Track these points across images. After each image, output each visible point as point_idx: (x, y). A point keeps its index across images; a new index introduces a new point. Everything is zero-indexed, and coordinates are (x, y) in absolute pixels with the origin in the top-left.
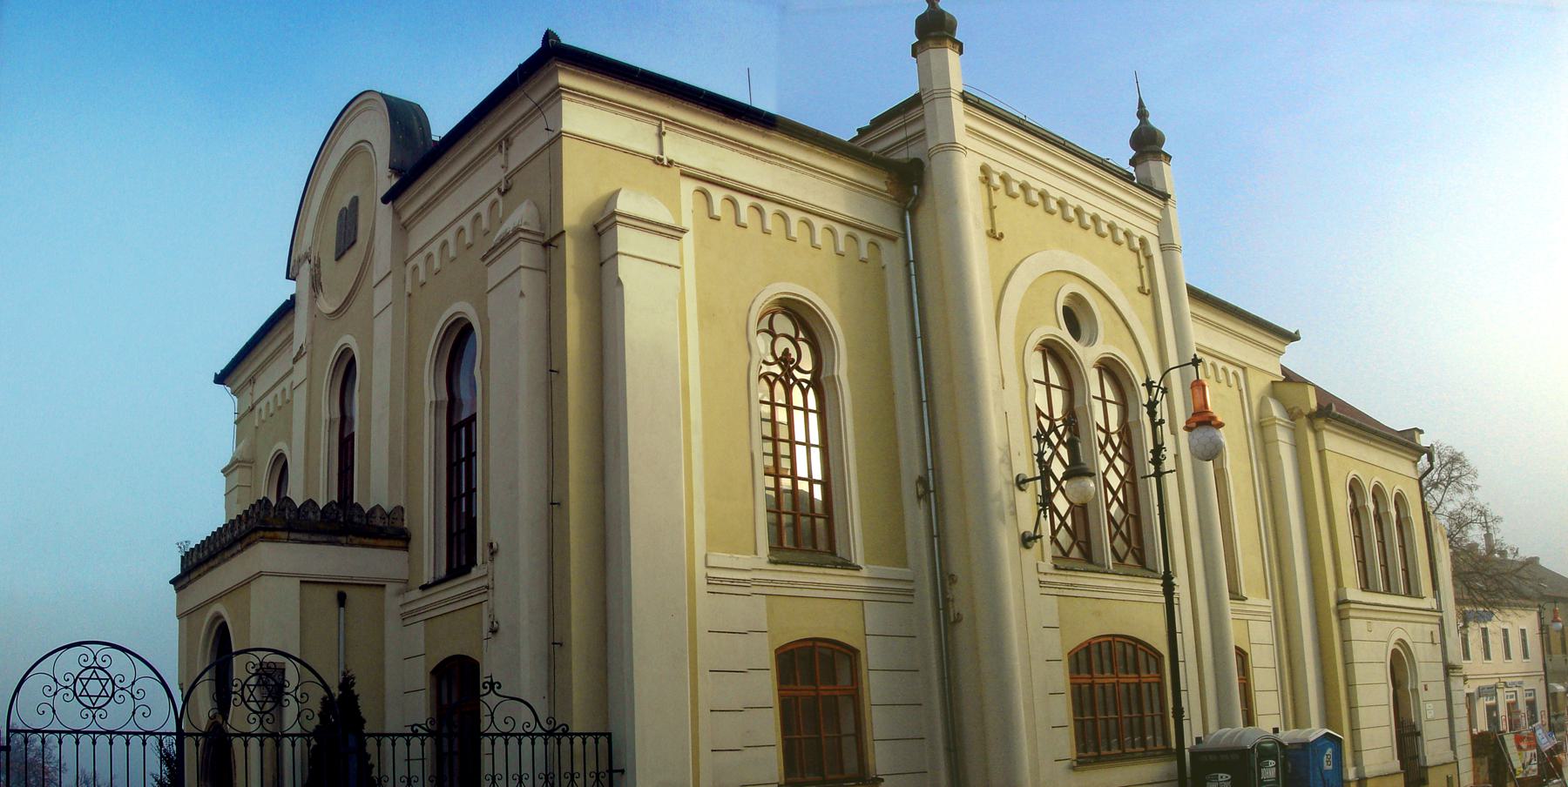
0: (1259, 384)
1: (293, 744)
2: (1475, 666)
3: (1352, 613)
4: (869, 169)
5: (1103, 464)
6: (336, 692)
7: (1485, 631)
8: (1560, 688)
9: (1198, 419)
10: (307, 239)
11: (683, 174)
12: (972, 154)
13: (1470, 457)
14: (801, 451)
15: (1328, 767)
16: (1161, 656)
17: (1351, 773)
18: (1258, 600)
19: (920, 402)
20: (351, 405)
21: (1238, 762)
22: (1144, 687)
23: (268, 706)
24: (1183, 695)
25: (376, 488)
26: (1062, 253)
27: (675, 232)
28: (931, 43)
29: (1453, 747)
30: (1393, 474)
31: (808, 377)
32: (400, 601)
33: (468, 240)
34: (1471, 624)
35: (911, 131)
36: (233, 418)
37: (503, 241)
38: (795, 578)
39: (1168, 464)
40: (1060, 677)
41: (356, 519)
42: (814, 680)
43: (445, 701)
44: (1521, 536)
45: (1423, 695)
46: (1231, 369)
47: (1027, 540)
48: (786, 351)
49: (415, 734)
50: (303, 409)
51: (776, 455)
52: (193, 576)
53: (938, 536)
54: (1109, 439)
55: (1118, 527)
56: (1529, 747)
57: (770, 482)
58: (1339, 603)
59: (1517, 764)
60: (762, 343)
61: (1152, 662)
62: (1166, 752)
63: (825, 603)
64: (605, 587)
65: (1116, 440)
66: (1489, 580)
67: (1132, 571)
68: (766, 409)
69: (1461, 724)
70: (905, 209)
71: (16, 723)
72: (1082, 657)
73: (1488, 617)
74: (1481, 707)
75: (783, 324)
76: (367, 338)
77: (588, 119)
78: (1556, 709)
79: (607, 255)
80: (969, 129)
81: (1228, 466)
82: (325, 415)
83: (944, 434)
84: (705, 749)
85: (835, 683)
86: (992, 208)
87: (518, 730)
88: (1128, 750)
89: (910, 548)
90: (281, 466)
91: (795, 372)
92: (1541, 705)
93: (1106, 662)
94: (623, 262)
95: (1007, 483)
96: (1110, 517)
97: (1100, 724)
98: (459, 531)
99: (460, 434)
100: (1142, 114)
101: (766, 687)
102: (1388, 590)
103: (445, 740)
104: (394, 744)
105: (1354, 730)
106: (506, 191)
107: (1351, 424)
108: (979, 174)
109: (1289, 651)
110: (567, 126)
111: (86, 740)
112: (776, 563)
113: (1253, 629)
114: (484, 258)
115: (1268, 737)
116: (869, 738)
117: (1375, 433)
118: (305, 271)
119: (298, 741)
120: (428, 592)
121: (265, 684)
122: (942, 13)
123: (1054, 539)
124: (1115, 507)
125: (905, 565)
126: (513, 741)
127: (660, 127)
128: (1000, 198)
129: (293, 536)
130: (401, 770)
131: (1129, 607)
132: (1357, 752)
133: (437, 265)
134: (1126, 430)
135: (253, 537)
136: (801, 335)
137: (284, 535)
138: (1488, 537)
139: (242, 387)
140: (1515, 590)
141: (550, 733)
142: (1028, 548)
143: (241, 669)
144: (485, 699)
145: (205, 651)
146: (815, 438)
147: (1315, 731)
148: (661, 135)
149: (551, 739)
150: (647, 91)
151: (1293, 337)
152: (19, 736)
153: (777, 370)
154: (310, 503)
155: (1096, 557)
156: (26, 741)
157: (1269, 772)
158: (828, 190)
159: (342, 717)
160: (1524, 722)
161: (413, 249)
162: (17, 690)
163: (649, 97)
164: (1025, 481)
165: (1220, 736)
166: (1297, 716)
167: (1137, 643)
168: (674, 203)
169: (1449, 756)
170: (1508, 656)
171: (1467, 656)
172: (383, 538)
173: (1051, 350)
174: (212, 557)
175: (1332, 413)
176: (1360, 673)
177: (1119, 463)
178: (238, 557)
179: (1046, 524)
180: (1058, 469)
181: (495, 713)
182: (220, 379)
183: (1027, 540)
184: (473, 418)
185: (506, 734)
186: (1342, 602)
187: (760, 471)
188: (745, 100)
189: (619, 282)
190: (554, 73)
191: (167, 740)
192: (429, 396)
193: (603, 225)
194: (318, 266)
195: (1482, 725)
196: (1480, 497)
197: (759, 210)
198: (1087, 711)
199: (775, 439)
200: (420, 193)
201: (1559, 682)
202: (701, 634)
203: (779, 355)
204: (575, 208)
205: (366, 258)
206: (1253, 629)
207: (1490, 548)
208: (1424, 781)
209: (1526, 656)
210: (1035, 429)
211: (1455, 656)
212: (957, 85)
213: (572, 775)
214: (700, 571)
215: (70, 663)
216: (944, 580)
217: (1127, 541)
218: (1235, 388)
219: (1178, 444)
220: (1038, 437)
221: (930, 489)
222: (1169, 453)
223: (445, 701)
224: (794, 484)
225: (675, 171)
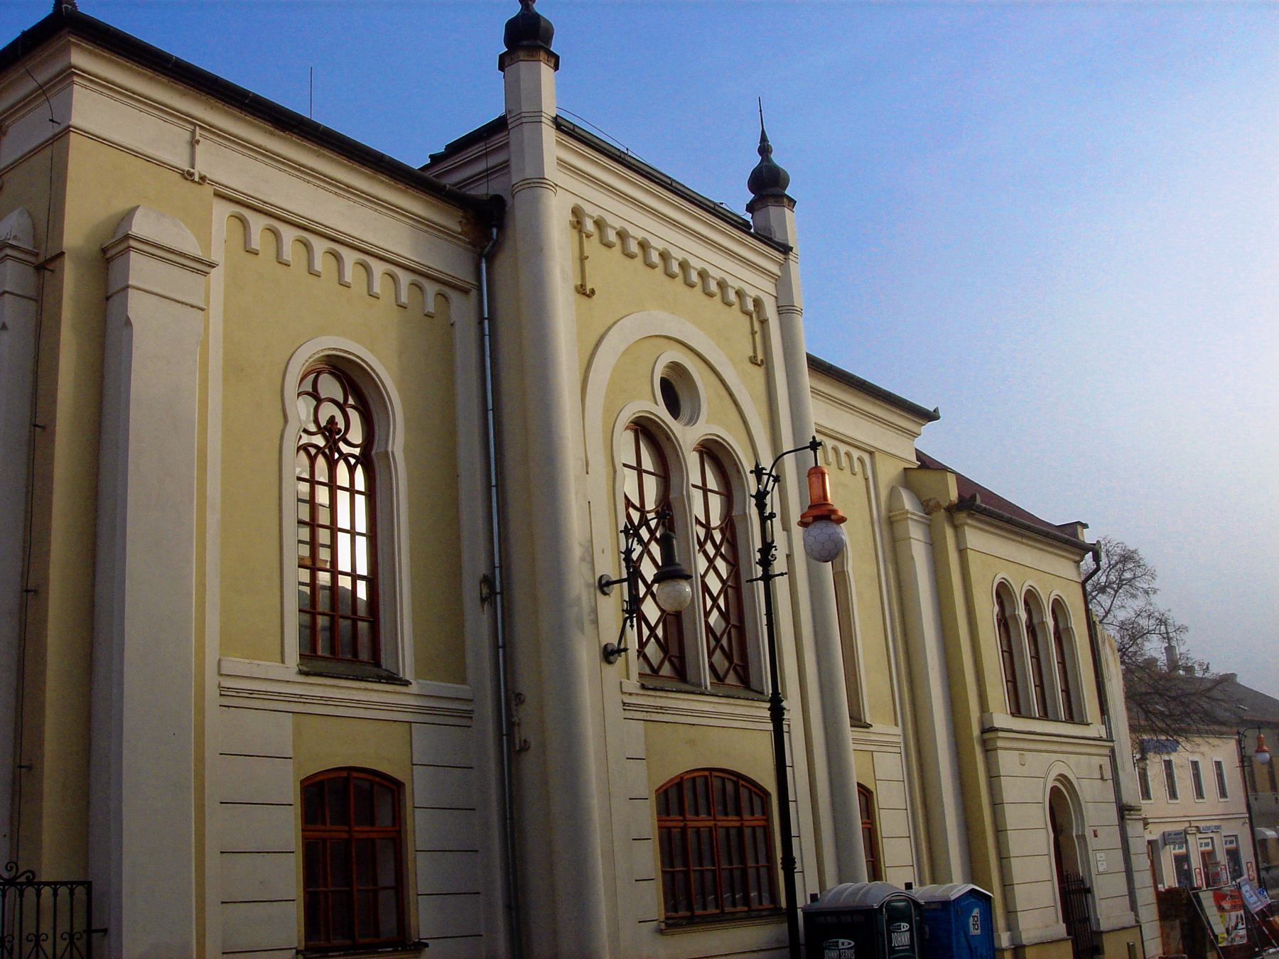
0: (888, 472)
2: (1157, 806)
3: (1000, 743)
4: (441, 204)
5: (702, 564)
7: (1168, 764)
8: (1270, 833)
9: (816, 512)
11: (218, 195)
12: (563, 188)
13: (1145, 554)
14: (344, 540)
15: (975, 931)
16: (768, 794)
17: (1004, 940)
18: (886, 727)
19: (489, 486)
21: (864, 924)
22: (748, 832)
24: (795, 842)
27: (202, 266)
28: (522, 55)
29: (1134, 907)
30: (1052, 576)
31: (357, 451)
34: (1150, 755)
35: (493, 161)
38: (329, 693)
39: (779, 565)
40: (646, 819)
42: (347, 818)
44: (1211, 649)
45: (1092, 843)
46: (856, 454)
47: (609, 654)
48: (332, 420)
51: (313, 544)
53: (503, 647)
54: (709, 535)
55: (718, 640)
56: (1234, 908)
57: (305, 575)
58: (984, 731)
59: (1219, 929)
60: (302, 409)
62: (774, 913)
63: (364, 725)
65: (718, 537)
66: (1173, 702)
67: (734, 692)
68: (304, 488)
69: (1143, 878)
70: (480, 256)
72: (673, 795)
73: (1173, 747)
74: (1167, 858)
75: (330, 387)
77: (107, 115)
78: (1266, 859)
79: (114, 288)
80: (562, 163)
81: (850, 568)
83: (515, 524)
84: (212, 896)
85: (373, 824)
86: (583, 259)
88: (728, 909)
89: (469, 660)
91: (342, 446)
92: (1247, 855)
93: (702, 802)
95: (588, 585)
96: (709, 629)
97: (694, 877)
100: (764, 150)
101: (286, 827)
102: (1045, 716)
105: (1007, 885)
107: (1000, 518)
108: (570, 217)
109: (923, 789)
112: (307, 674)
113: (880, 763)
115: (899, 894)
116: (412, 892)
117: (1028, 528)
122: (537, 17)
123: (641, 653)
124: (714, 617)
125: (463, 681)
127: (193, 132)
128: (593, 246)
131: (728, 734)
132: (1010, 913)
134: (729, 525)
136: (351, 401)
138: (1170, 650)
140: (1206, 713)
142: (610, 663)
146: (361, 526)
147: (958, 887)
148: (193, 143)
151: (931, 416)
153: (320, 441)
155: (690, 674)
157: (902, 938)
158: (392, 228)
160: (1225, 875)
164: (609, 583)
165: (840, 893)
166: (935, 868)
167: (739, 779)
169: (1128, 919)
170: (1200, 794)
171: (1146, 794)
173: (645, 429)
175: (977, 505)
176: (1012, 816)
177: (721, 565)
179: (632, 635)
180: (648, 570)
183: (609, 654)
186: (988, 729)
187: (291, 562)
189: (128, 323)
190: (66, 50)
193: (112, 250)
195: (1170, 880)
196: (1160, 603)
197: (307, 245)
198: (678, 861)
199: (313, 525)
201: (1269, 826)
203: (323, 424)
204: (79, 227)
206: (880, 763)
207: (1173, 664)
208: (1098, 950)
209: (1223, 793)
210: (623, 521)
211: (1131, 791)
212: (550, 108)
213: (38, 936)
216: (509, 701)
217: (728, 656)
218: (860, 477)
219: (791, 543)
220: (626, 531)
221: (496, 590)
222: (780, 553)
224: (334, 579)
225: (208, 190)
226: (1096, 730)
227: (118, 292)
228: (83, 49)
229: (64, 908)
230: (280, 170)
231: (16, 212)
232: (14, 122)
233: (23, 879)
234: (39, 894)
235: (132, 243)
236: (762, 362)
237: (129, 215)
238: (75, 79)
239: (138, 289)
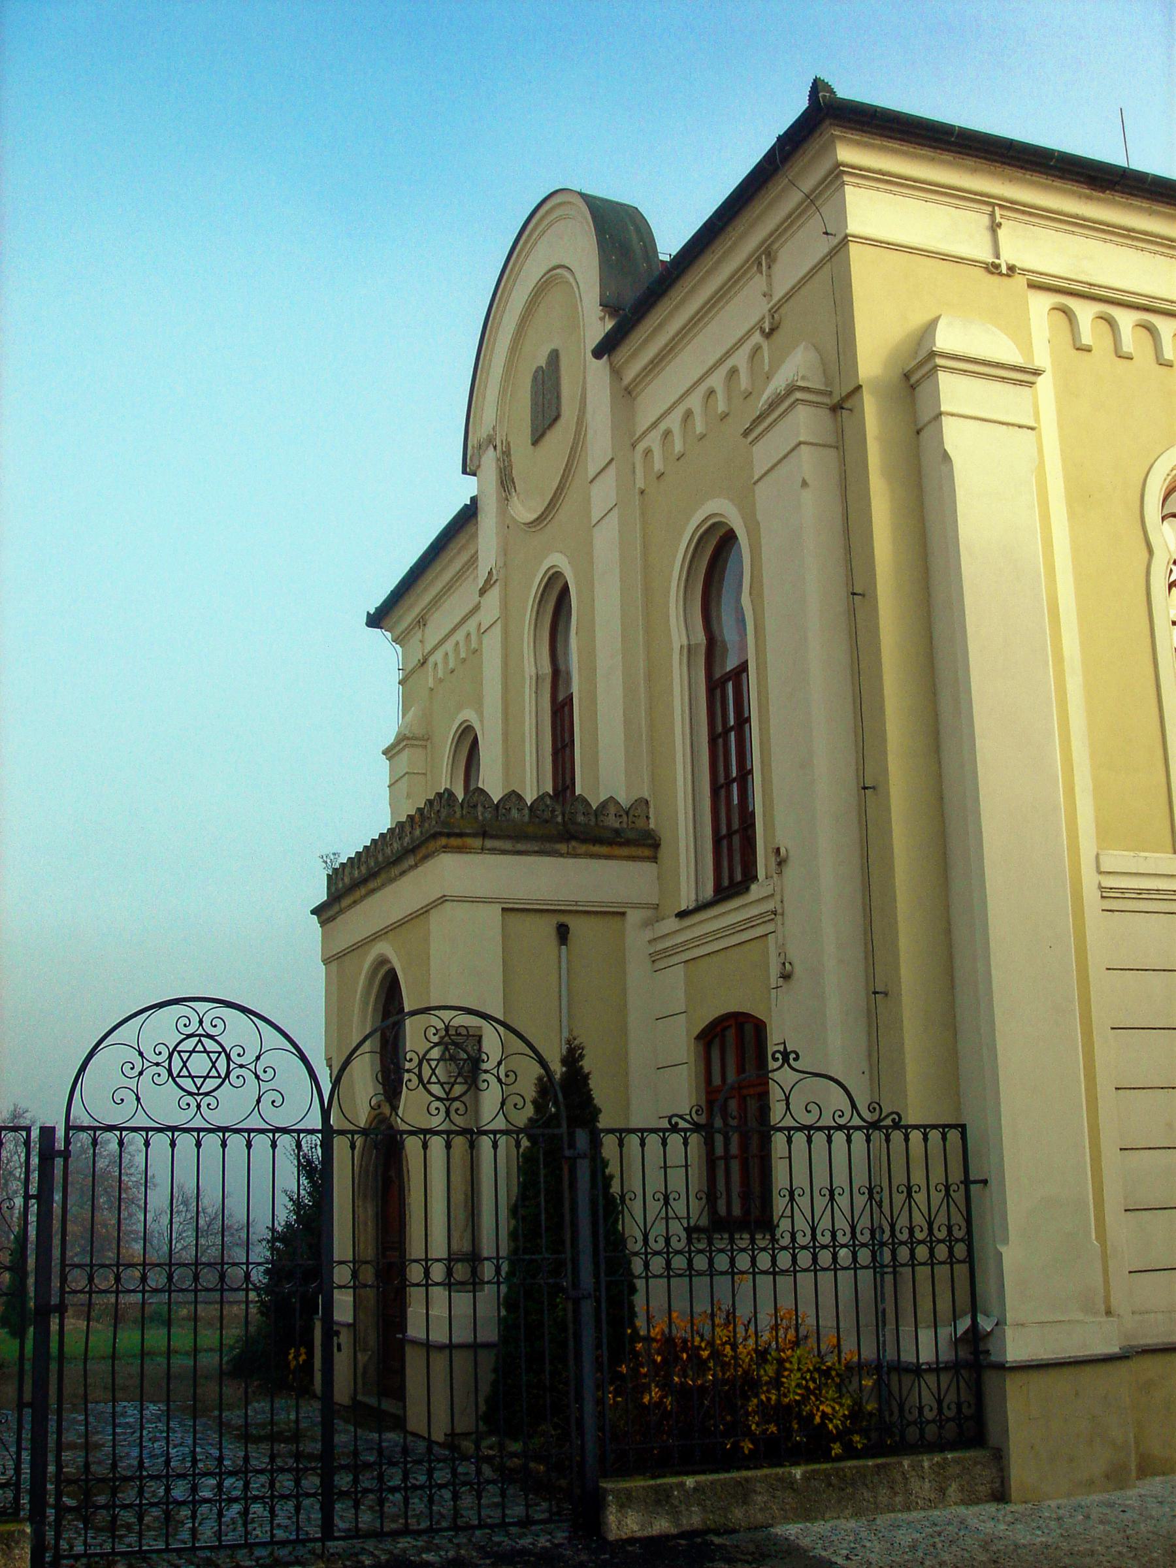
1: (495, 1145)
6: (558, 1069)
10: (488, 415)
11: (1032, 285)
20: (566, 654)
23: (458, 1090)
25: (608, 773)
27: (1024, 375)
32: (648, 934)
33: (721, 407)
36: (396, 676)
37: (772, 405)
41: (581, 819)
43: (717, 1081)
49: (674, 1129)
50: (498, 662)
52: (345, 902)
64: (947, 907)
71: (80, 1116)
76: (584, 555)
77: (887, 213)
79: (925, 417)
82: (529, 669)
87: (826, 1121)
90: (469, 746)
94: (950, 427)
98: (730, 835)
99: (725, 694)
103: (719, 1139)
104: (643, 1144)
106: (772, 330)
110: (855, 225)
111: (186, 1141)
114: (746, 434)
118: (489, 460)
119: (502, 1140)
120: (688, 922)
121: (452, 1058)
126: (819, 1138)
127: (992, 215)
129: (489, 843)
130: (655, 1183)
133: (678, 447)
135: (432, 845)
137: (477, 843)
139: (408, 631)
141: (875, 1125)
143: (417, 1037)
144: (776, 1076)
145: (364, 1010)
148: (994, 227)
149: (877, 1136)
150: (970, 162)
152: (84, 1136)
154: (513, 797)
156: (95, 1142)
159: (568, 1101)
161: (643, 422)
162: (83, 1068)
163: (974, 171)
168: (1021, 333)
172: (621, 844)
174: (373, 875)
178: (412, 875)
181: (792, 1096)
182: (376, 620)
184: (743, 667)
185: (809, 1128)
188: (1119, 160)
189: (946, 457)
190: (829, 147)
191: (307, 1141)
192: (678, 637)
193: (917, 372)
194: (507, 453)
200: (646, 341)
202: (1096, 973)
204: (874, 351)
205: (578, 433)
213: (909, 1189)
214: (1090, 881)
215: (163, 1029)
223: (717, 1081)
225: (1020, 281)
227: (930, 422)
228: (850, 142)
229: (827, 1300)
230: (1105, 241)
231: (802, 347)
232: (782, 246)
233: (888, 1122)
234: (907, 1139)
235: (940, 361)
237: (930, 328)
238: (846, 178)
239: (952, 415)
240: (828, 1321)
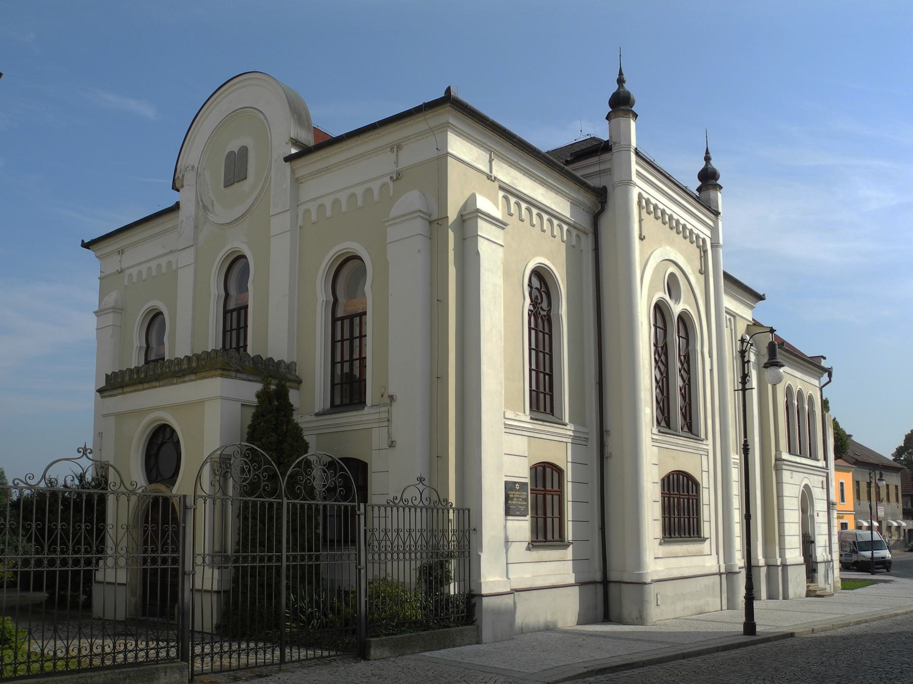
11: (501, 188)
26: (668, 248)
29: (831, 552)
35: (603, 167)
58: (776, 460)
61: (556, 475)
100: (621, 81)
102: (801, 455)
129: (239, 375)
137: (233, 374)
148: (491, 161)
151: (761, 298)
186: (778, 459)
189: (478, 253)
225: (496, 184)
226: (821, 463)
236: (704, 272)
240: (407, 580)
